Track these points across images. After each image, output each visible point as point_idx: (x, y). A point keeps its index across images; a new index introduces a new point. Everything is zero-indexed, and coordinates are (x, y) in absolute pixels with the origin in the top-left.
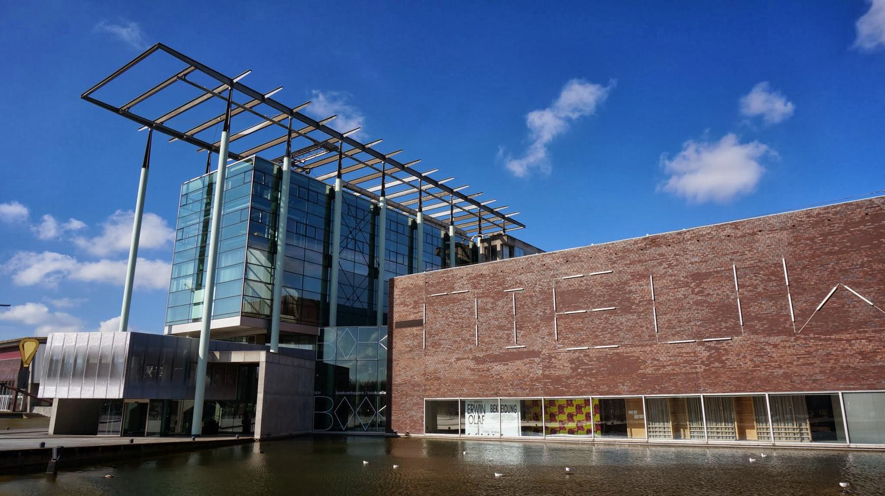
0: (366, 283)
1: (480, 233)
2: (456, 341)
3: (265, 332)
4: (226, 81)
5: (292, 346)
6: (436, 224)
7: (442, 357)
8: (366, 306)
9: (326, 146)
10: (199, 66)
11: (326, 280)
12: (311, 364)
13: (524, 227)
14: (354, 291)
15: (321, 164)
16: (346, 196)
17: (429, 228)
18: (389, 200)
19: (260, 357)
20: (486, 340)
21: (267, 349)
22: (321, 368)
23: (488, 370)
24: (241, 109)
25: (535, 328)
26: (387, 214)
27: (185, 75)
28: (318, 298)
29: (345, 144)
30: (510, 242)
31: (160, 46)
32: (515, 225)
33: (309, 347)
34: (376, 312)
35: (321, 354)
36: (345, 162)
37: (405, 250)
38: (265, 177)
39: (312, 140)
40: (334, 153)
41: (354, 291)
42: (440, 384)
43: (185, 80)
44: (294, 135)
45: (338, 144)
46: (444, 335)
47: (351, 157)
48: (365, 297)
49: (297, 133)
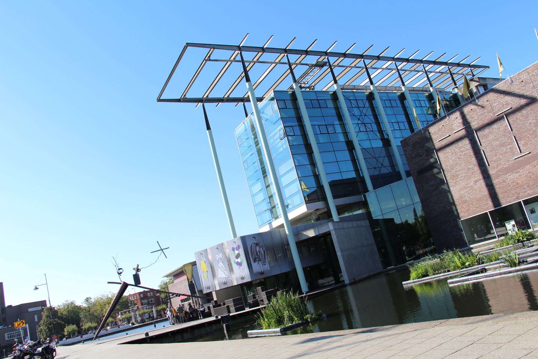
0: (384, 153)
1: (455, 84)
2: (470, 169)
3: (326, 210)
4: (235, 48)
5: (347, 215)
6: (419, 91)
7: (463, 184)
8: (389, 168)
9: (320, 65)
10: (215, 47)
11: (354, 160)
12: (366, 223)
13: (488, 67)
14: (377, 161)
15: (320, 78)
16: (345, 94)
17: (415, 95)
18: (378, 86)
19: (330, 227)
20: (494, 159)
21: (332, 221)
22: (374, 223)
23: (504, 181)
24: (252, 64)
25: (532, 134)
26: (380, 97)
27: (209, 57)
28: (353, 175)
29: (330, 58)
30: (482, 82)
31: (188, 45)
32: (481, 69)
33: (360, 212)
34: (399, 172)
35: (369, 214)
36: (336, 71)
37: (403, 118)
38: (288, 102)
39: (306, 65)
40: (325, 68)
41: (377, 161)
42: (468, 205)
43: (210, 60)
44: (293, 67)
45: (326, 60)
46: (458, 168)
47: (338, 66)
48: (386, 162)
49: (295, 63)
